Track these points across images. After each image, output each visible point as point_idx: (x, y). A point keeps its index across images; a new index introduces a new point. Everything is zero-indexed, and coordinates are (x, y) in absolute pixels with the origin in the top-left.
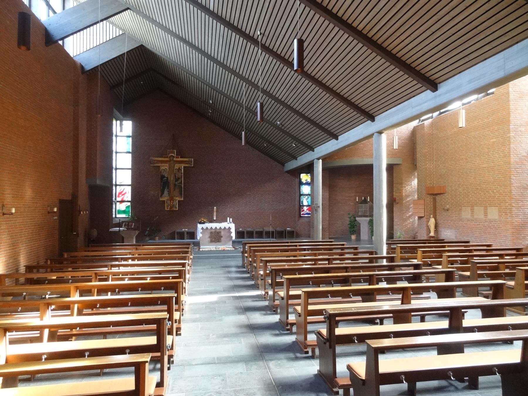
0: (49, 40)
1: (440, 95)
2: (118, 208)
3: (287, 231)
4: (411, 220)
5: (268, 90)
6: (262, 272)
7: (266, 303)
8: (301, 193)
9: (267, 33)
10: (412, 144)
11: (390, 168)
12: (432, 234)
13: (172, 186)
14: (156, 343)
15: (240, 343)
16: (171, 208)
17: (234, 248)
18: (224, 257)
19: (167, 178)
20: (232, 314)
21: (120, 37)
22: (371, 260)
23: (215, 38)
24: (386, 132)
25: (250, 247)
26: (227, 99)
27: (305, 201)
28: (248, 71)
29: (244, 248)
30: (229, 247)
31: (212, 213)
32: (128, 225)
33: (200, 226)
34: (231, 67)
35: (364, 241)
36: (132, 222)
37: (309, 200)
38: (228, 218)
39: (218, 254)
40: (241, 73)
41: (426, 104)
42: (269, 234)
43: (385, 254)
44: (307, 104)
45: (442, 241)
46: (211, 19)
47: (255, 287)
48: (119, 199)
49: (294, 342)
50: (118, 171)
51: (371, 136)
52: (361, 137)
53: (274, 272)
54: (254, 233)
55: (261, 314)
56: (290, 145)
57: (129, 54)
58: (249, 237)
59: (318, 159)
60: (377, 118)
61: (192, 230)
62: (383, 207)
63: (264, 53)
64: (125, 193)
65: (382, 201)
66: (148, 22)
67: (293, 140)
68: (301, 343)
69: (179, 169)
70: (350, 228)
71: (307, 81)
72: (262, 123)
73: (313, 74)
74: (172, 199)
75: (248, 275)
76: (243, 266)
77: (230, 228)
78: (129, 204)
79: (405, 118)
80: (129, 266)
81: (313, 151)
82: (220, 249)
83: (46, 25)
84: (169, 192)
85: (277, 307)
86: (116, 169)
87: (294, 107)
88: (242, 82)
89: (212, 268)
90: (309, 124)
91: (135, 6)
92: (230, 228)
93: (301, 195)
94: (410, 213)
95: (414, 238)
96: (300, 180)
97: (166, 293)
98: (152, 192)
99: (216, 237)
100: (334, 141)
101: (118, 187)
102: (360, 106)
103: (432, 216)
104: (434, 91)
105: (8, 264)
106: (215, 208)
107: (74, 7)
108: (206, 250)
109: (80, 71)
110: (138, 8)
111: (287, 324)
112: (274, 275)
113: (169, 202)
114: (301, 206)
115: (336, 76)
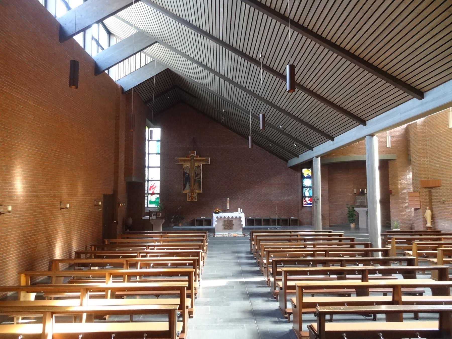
0: (98, 71)
1: (426, 103)
2: (149, 200)
3: (292, 218)
4: (407, 211)
5: (270, 101)
6: (265, 261)
7: (268, 290)
8: (303, 186)
9: (267, 56)
10: (405, 144)
11: (384, 165)
12: (429, 225)
13: (192, 181)
14: (168, 329)
15: (243, 328)
16: (192, 199)
17: (244, 234)
18: (235, 243)
19: (189, 174)
20: (238, 299)
21: (151, 64)
22: (366, 253)
23: (225, 61)
24: (377, 134)
25: (257, 236)
26: (237, 109)
27: (307, 193)
28: (253, 86)
29: (252, 236)
30: (239, 234)
31: (226, 204)
32: (156, 215)
33: (215, 216)
34: (239, 83)
35: (362, 229)
36: (159, 212)
37: (311, 192)
38: (239, 209)
39: (231, 240)
40: (247, 87)
41: (414, 111)
42: (275, 222)
43: (380, 247)
44: (305, 111)
45: (438, 233)
46: (221, 47)
47: (259, 273)
48: (150, 192)
49: (291, 331)
50: (149, 169)
51: (364, 138)
52: (355, 139)
53: (274, 263)
54: (262, 221)
55: (263, 300)
56: (292, 145)
57: (158, 76)
58: (258, 225)
59: (317, 157)
60: (368, 123)
61: (209, 218)
62: (376, 202)
63: (265, 72)
64: (156, 187)
65: (375, 197)
66: (172, 51)
67: (294, 141)
68: (296, 331)
69: (198, 167)
70: (349, 217)
71: (303, 93)
72: (264, 131)
73: (308, 87)
74: (192, 191)
75: (254, 261)
76: (251, 252)
77: (240, 218)
78: (158, 196)
79: (394, 123)
80: (156, 249)
81: (312, 150)
82: (232, 236)
83: (95, 60)
84: (190, 186)
85: (277, 295)
86: (148, 167)
87: (294, 114)
88: (248, 95)
89: (224, 253)
90: (307, 128)
91: (161, 40)
92: (240, 218)
93: (303, 187)
94: (406, 205)
95: (411, 228)
96: (302, 174)
97: (188, 269)
98: (177, 186)
99: (229, 224)
100: (330, 142)
101: (150, 182)
102: (352, 112)
103: (428, 208)
104: (420, 99)
105: (64, 247)
106: (228, 199)
107: (117, 44)
108: (220, 236)
109: (121, 92)
110: (164, 41)
111: (286, 313)
112: (274, 266)
113: (190, 194)
114: (303, 197)
115: (329, 88)
